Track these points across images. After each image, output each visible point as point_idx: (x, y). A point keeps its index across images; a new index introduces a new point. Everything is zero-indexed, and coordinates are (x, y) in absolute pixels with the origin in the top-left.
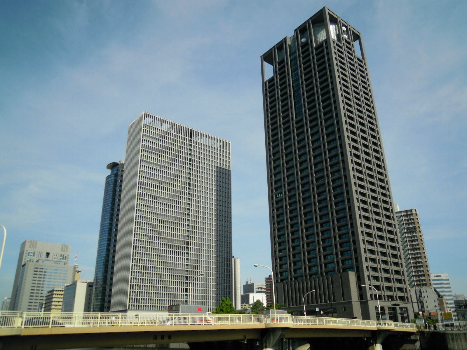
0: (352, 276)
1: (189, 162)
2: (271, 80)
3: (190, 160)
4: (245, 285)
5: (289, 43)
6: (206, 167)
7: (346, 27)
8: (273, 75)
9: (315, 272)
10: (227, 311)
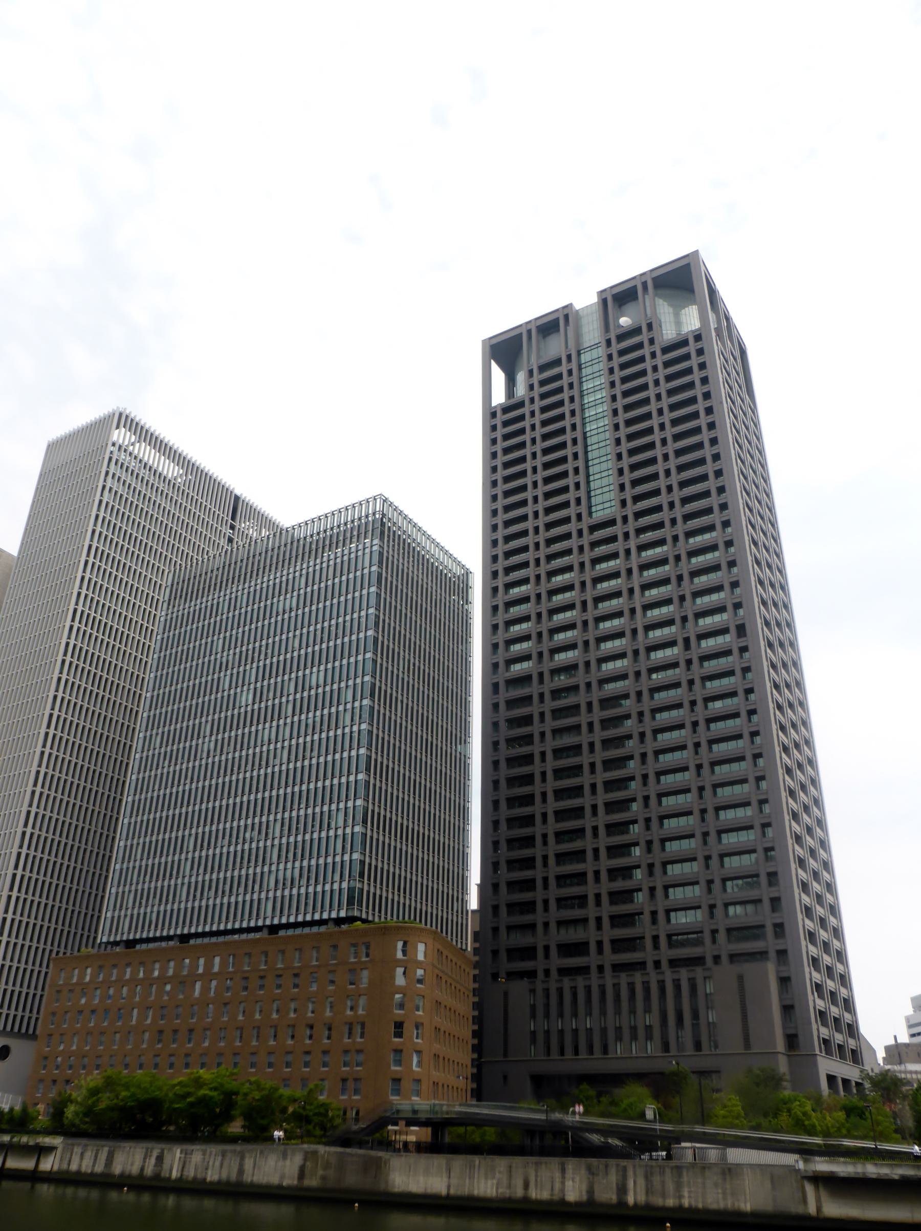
2: (506, 409)
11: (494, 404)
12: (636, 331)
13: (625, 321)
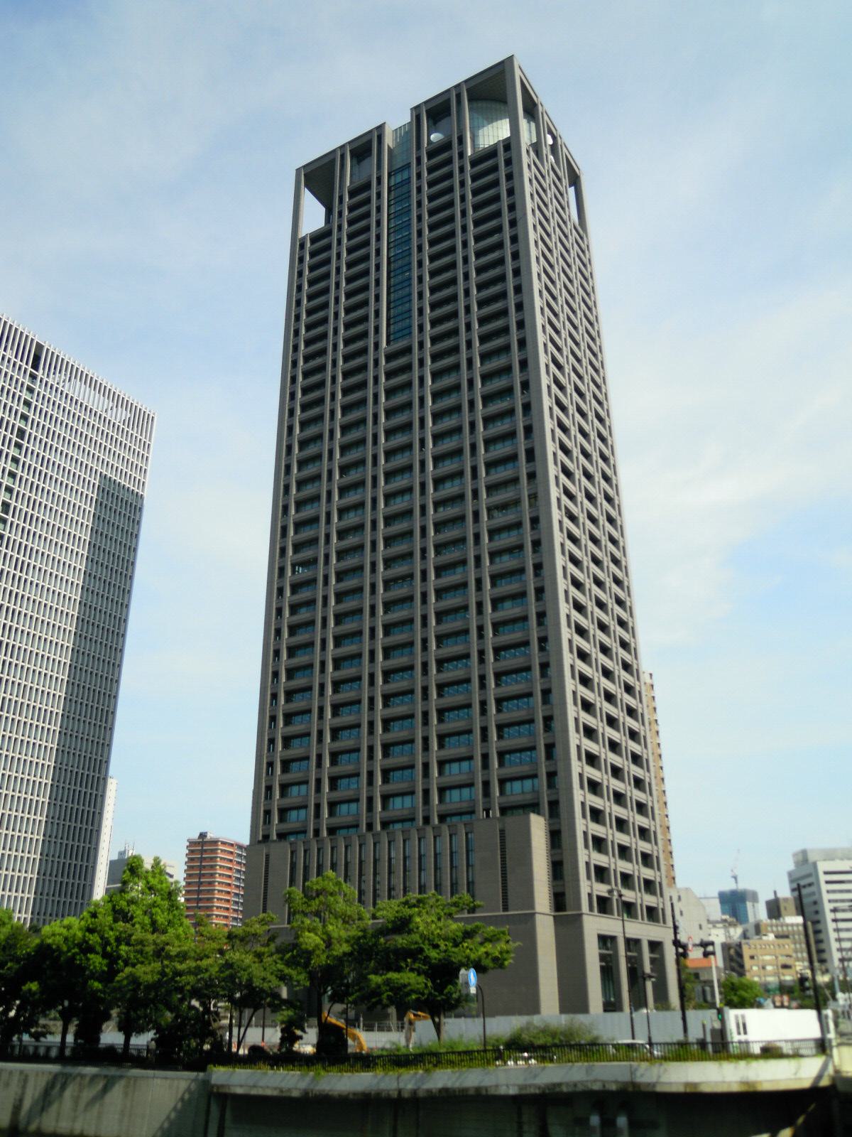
0: (538, 826)
1: (15, 438)
2: (316, 237)
3: (21, 433)
4: (115, 861)
5: (389, 141)
6: (58, 557)
7: (554, 138)
9: (406, 812)
10: (154, 923)
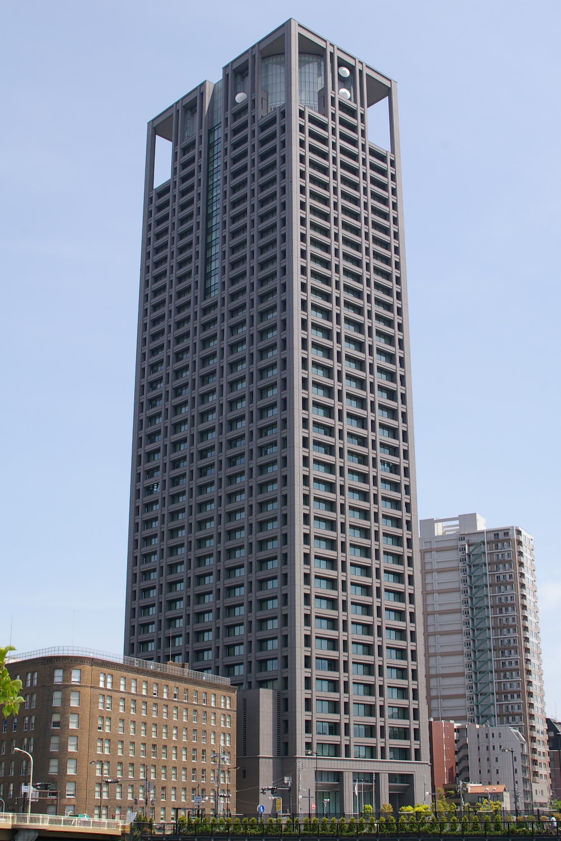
2: (165, 190)
7: (352, 69)
8: (170, 178)
11: (155, 187)
12: (244, 109)
13: (240, 97)
